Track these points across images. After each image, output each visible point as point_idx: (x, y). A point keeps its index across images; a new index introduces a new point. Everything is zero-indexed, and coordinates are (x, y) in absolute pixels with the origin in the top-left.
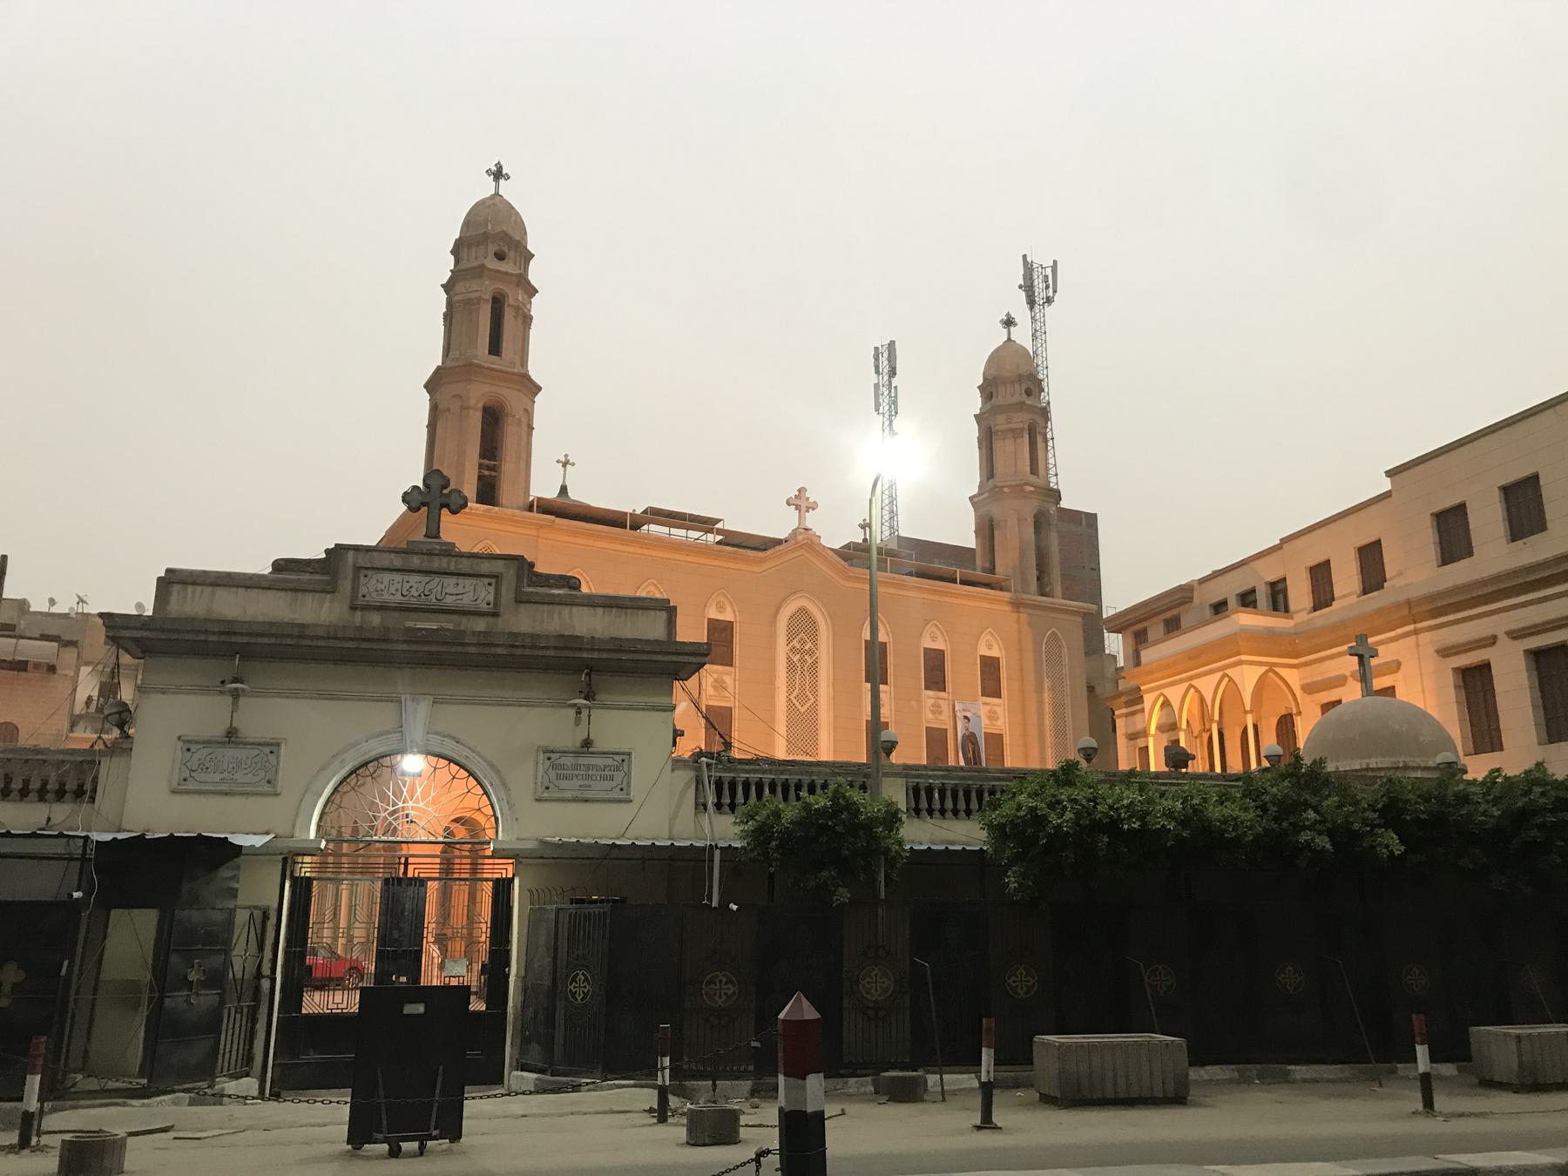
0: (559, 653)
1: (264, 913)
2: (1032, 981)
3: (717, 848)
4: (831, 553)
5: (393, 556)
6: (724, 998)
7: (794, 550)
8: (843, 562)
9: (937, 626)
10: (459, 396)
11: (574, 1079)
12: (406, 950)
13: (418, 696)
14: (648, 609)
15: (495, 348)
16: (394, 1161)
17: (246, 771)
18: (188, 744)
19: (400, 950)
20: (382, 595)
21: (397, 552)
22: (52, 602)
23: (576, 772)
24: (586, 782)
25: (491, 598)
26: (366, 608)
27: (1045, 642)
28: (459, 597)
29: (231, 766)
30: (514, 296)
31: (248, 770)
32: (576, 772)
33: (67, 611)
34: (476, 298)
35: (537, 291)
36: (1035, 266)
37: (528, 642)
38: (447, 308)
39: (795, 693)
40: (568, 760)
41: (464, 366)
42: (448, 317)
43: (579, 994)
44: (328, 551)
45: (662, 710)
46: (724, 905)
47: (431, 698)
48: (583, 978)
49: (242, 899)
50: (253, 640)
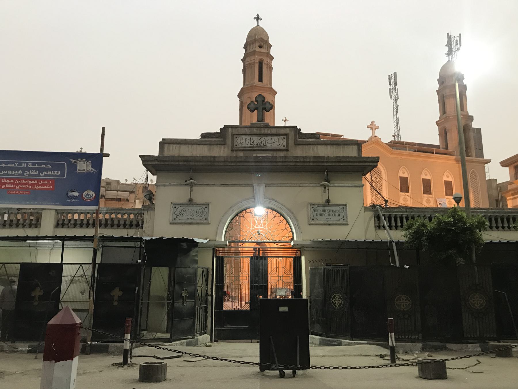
0: (315, 164)
1: (207, 270)
2: (333, 301)
3: (393, 242)
4: (385, 145)
5: (246, 129)
6: (405, 306)
7: (371, 144)
8: (390, 148)
9: (427, 170)
10: (249, 97)
11: (338, 339)
12: (261, 285)
13: (260, 184)
14: (349, 145)
15: (261, 80)
16: (282, 379)
17: (197, 215)
18: (175, 205)
19: (259, 285)
20: (243, 145)
21: (248, 128)
22: (126, 180)
23: (325, 213)
24: (328, 217)
25: (285, 144)
26: (238, 150)
27: (470, 174)
28: (273, 144)
29: (191, 213)
30: (266, 60)
31: (198, 215)
32: (325, 213)
33: (131, 183)
34: (253, 63)
35: (274, 58)
36: (452, 37)
37: (302, 160)
38: (243, 67)
39: (374, 196)
40: (321, 208)
41: (251, 87)
42: (244, 71)
43: (337, 304)
44: (221, 129)
45: (358, 187)
46: (402, 266)
47: (265, 184)
48: (338, 297)
49: (200, 264)
50: (196, 164)
